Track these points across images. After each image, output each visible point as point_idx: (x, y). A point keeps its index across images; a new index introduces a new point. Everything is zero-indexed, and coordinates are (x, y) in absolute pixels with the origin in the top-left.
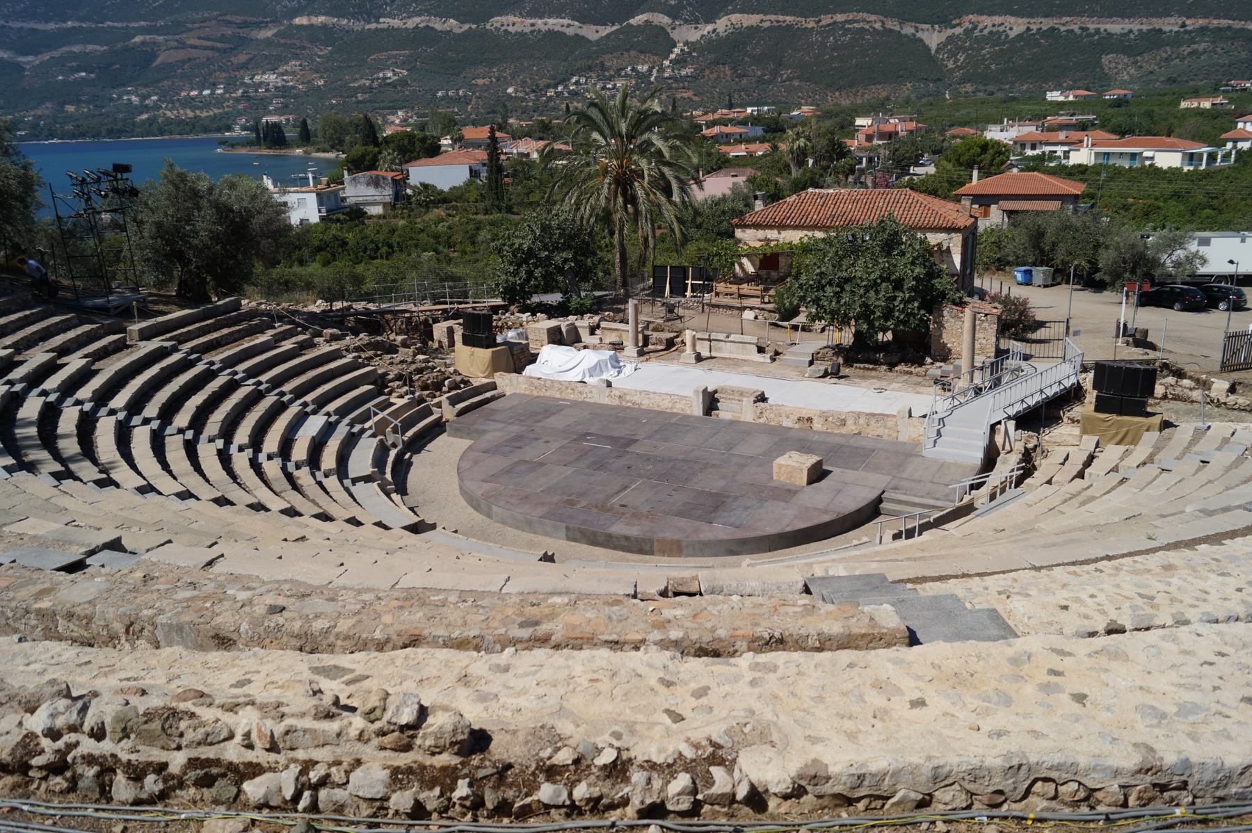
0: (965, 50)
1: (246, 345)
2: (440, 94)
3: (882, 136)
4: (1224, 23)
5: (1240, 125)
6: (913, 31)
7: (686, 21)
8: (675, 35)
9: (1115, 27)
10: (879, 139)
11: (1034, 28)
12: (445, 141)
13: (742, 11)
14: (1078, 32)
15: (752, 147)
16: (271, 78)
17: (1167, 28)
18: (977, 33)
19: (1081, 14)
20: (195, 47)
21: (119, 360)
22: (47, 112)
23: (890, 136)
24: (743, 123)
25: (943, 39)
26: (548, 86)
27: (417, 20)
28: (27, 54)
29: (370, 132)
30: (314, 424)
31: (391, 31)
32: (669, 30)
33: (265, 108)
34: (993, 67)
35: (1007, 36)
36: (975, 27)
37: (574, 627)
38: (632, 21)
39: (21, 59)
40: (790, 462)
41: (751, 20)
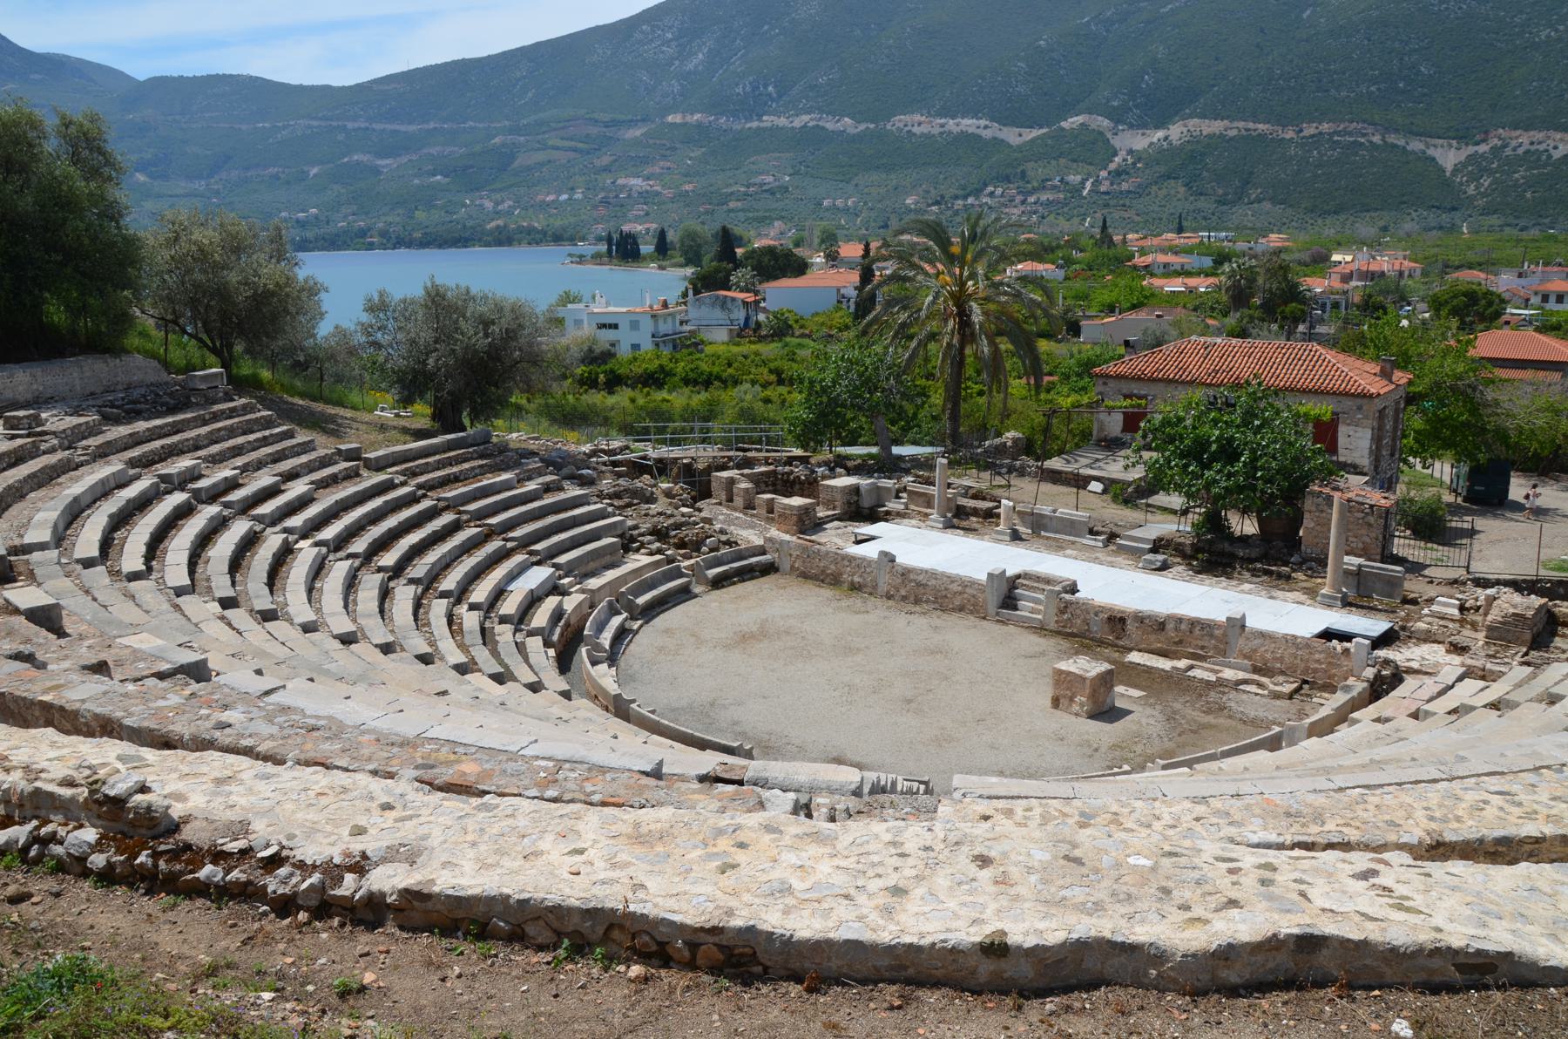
0: (1491, 172)
1: (485, 482)
6: (1422, 147)
7: (1131, 126)
8: (1116, 142)
10: (1359, 279)
13: (1203, 116)
15: (1192, 282)
18: (1508, 152)
20: (557, 148)
22: (398, 219)
24: (1188, 251)
25: (1463, 158)
26: (956, 197)
27: (806, 118)
28: (387, 156)
29: (727, 241)
30: (538, 576)
31: (774, 130)
32: (1109, 136)
33: (625, 215)
34: (1528, 195)
35: (1550, 157)
36: (1505, 146)
38: (1064, 124)
40: (1073, 669)
41: (1216, 126)
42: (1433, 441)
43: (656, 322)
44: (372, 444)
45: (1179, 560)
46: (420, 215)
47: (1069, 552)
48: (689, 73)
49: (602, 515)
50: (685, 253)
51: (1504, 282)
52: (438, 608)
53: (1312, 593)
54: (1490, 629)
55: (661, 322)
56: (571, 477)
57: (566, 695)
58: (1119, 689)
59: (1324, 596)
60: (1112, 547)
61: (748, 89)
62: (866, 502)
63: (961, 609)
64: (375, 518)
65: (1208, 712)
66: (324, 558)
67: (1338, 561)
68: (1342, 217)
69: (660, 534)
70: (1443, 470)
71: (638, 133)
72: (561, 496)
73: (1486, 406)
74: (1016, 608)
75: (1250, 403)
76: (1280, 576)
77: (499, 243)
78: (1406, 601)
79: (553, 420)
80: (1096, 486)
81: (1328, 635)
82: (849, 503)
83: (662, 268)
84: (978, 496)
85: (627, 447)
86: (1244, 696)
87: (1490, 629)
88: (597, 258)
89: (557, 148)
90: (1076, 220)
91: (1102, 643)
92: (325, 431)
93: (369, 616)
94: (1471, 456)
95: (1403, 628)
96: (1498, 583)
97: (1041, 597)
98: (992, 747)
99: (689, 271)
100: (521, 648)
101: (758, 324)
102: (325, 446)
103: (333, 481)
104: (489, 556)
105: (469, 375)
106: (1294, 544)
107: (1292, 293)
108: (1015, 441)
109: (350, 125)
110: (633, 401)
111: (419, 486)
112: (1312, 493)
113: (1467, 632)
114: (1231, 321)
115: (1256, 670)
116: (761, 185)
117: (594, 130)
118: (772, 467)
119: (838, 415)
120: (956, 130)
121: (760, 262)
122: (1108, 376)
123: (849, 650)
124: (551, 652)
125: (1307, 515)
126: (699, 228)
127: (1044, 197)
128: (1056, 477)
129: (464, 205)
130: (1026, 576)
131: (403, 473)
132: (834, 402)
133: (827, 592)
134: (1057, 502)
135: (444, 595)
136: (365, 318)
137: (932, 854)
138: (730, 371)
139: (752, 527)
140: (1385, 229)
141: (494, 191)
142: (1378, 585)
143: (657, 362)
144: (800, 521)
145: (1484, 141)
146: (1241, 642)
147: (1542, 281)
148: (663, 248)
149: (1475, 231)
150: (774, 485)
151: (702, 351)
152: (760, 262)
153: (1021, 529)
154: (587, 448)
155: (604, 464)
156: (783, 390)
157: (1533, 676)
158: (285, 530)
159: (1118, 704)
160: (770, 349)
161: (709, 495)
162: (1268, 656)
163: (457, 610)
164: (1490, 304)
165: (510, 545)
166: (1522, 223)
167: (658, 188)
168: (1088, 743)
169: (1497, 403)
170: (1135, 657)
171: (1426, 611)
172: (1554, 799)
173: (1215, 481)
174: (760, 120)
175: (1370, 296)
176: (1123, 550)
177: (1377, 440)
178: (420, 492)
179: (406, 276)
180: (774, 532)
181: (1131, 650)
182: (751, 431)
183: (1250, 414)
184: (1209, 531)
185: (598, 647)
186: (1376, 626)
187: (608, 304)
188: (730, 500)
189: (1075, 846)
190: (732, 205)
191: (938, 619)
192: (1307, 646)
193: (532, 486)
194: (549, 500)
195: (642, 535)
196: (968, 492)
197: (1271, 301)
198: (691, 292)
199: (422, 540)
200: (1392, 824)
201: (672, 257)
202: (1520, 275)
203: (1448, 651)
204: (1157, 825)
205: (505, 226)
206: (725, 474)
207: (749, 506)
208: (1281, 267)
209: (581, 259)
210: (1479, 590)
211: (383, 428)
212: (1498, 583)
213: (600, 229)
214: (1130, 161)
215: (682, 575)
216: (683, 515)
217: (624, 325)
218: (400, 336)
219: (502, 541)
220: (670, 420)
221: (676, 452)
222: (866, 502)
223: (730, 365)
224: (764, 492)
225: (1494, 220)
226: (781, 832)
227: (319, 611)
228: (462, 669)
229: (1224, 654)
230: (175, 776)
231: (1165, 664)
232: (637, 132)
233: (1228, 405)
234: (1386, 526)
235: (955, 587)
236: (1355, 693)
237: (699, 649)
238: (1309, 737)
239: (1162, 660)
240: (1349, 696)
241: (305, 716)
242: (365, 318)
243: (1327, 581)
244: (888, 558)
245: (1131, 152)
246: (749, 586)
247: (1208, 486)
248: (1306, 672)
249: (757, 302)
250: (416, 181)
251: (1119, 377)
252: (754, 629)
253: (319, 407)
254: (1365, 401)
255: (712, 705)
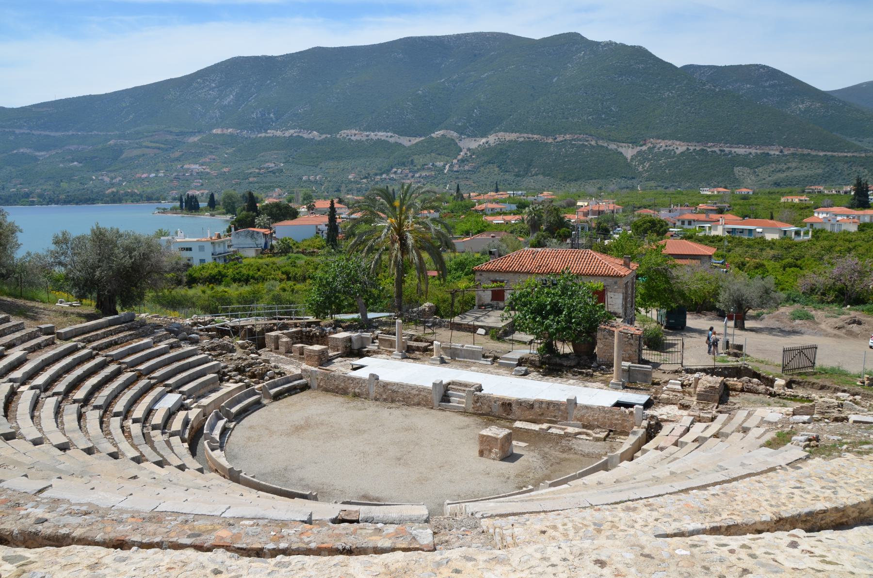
0: (649, 160)
1: (134, 345)
2: (304, 178)
3: (594, 213)
4: (806, 151)
5: (816, 215)
7: (469, 136)
8: (461, 144)
9: (741, 151)
11: (692, 148)
12: (303, 209)
13: (505, 131)
14: (719, 152)
15: (508, 218)
16: (196, 167)
17: (772, 153)
18: (656, 150)
19: (719, 142)
20: (148, 147)
21: (46, 352)
22: (50, 187)
23: (600, 213)
24: (503, 201)
26: (376, 174)
27: (292, 131)
29: (251, 201)
30: (171, 399)
32: (457, 141)
33: (189, 186)
35: (675, 153)
36: (654, 147)
37: (222, 538)
38: (433, 135)
39: (37, 154)
40: (490, 434)
41: (512, 136)
42: (649, 299)
43: (214, 246)
44: (61, 324)
45: (532, 369)
46: (64, 185)
47: (473, 368)
48: (225, 106)
49: (205, 361)
50: (226, 207)
51: (663, 214)
52: (115, 423)
53: (606, 383)
54: (699, 395)
55: (217, 246)
56: (185, 339)
57: (201, 470)
58: (514, 443)
59: (613, 384)
60: (496, 364)
61: (259, 115)
62: (356, 346)
63: (418, 404)
64: (68, 369)
65: (563, 452)
66: (38, 397)
67: (619, 365)
68: (579, 183)
69: (240, 370)
70: (654, 314)
71: (196, 139)
72: (180, 351)
73: (673, 278)
74: (449, 401)
75: (566, 284)
76: (587, 375)
77: (114, 202)
78: (654, 384)
79: (163, 306)
80: (481, 331)
81: (618, 404)
82: (346, 347)
83: (212, 215)
84: (417, 340)
85: (213, 320)
86: (581, 441)
87: (699, 395)
88: (174, 210)
89: (148, 147)
90: (441, 186)
91: (499, 418)
92: (26, 317)
93: (74, 431)
94: (668, 306)
95: (655, 398)
96: (697, 371)
97: (464, 394)
98: (451, 481)
99: (228, 217)
100: (168, 443)
101: (272, 247)
102: (30, 327)
103: (38, 348)
104: (141, 389)
105: (117, 282)
106: (594, 357)
107: (561, 223)
108: (430, 307)
109: (17, 131)
110: (204, 292)
111: (94, 349)
112: (601, 329)
113: (687, 398)
114: (532, 238)
115: (584, 427)
116: (268, 168)
117: (170, 137)
118: (299, 329)
119: (337, 298)
120: (375, 138)
121: (271, 211)
122: (482, 271)
123: (360, 432)
124: (186, 445)
125: (598, 341)
126: (233, 193)
127: (424, 174)
128: (459, 327)
129: (92, 180)
130: (453, 383)
131: (83, 341)
132: (334, 290)
133: (340, 399)
134: (462, 341)
135: (117, 415)
136: (53, 247)
137: (569, 563)
138: (259, 273)
139: (292, 363)
140: (600, 188)
141: (110, 171)
142: (639, 376)
143: (216, 270)
144: (320, 359)
145: (644, 144)
146: (575, 412)
147: (681, 214)
148: (212, 204)
149: (643, 189)
150: (301, 338)
151: (241, 262)
152: (271, 211)
153: (445, 357)
154: (188, 321)
155: (201, 330)
156: (290, 283)
157: (730, 419)
158: (11, 380)
159: (515, 451)
160: (280, 260)
161: (264, 346)
162: (590, 418)
163: (126, 423)
164: (662, 226)
165: (153, 381)
166: (666, 185)
167: (208, 170)
168: (503, 475)
169: (678, 278)
170: (518, 424)
171: (665, 388)
172: (823, 488)
173: (551, 326)
174: (266, 132)
175: (600, 223)
176: (502, 365)
177: (625, 299)
178: (95, 352)
179: (80, 222)
180: (304, 366)
181: (515, 421)
182: (282, 308)
183: (565, 289)
184: (547, 352)
185: (213, 440)
186: (643, 398)
187: (185, 237)
188: (277, 348)
189: (642, 548)
190: (251, 179)
191: (406, 411)
192: (611, 411)
193: (162, 345)
194: (173, 353)
195: (230, 371)
196: (411, 338)
197: (552, 228)
198: (233, 229)
199: (99, 382)
200: (753, 511)
201: (218, 209)
202: (670, 211)
203: (679, 409)
204: (637, 526)
205: (117, 191)
206: (273, 334)
207: (288, 351)
208: (555, 209)
209: (164, 211)
210: (689, 375)
211: (65, 314)
212: (697, 371)
213: (175, 193)
214: (469, 154)
215: (256, 394)
216: (252, 359)
217: (195, 249)
218: (75, 258)
219: (147, 380)
220: (230, 303)
221: (243, 322)
222: (356, 346)
223: (259, 270)
224: (296, 343)
225: (652, 184)
226: (475, 560)
227: (40, 430)
228: (138, 460)
229: (566, 419)
230: (57, 567)
231: (535, 427)
232: (195, 139)
233: (554, 284)
234: (640, 344)
235: (414, 392)
236: (640, 435)
237: (271, 435)
238: (621, 461)
239: (533, 425)
240: (636, 437)
241: (71, 504)
242: (53, 247)
243: (614, 375)
244: (374, 377)
245: (469, 149)
246: (295, 398)
247: (547, 328)
248: (612, 424)
249: (271, 234)
250: (61, 165)
251: (488, 271)
252: (302, 423)
253: (21, 302)
254: (619, 279)
255: (285, 470)
